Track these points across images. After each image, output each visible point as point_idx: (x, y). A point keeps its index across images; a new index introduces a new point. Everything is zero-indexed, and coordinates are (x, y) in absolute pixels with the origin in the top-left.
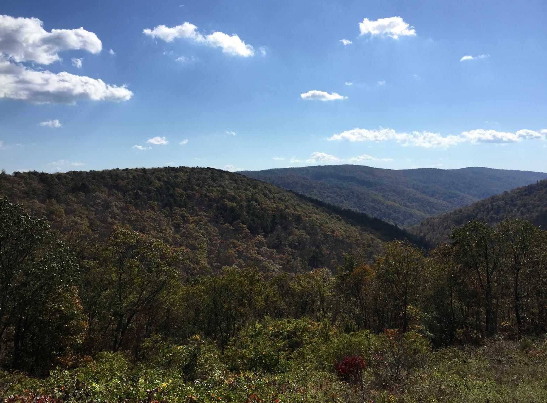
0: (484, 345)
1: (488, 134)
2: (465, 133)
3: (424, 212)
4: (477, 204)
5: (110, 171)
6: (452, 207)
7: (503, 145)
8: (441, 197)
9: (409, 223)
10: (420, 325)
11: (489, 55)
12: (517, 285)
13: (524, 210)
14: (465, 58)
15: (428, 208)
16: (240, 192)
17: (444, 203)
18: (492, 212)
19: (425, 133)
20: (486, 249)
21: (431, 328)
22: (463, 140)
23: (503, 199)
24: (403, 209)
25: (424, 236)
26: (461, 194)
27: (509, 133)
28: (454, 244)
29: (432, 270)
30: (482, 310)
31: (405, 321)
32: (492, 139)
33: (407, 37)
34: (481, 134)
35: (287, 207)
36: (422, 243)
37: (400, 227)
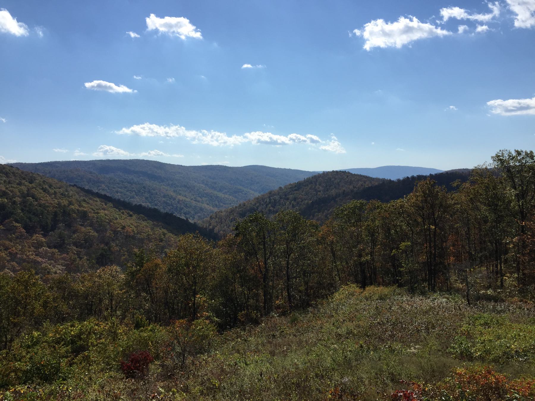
2: (247, 134)
3: (213, 206)
4: (258, 199)
7: (278, 146)
9: (199, 216)
12: (288, 268)
13: (295, 203)
14: (245, 66)
18: (270, 205)
19: (213, 133)
22: (246, 140)
24: (194, 203)
25: (213, 228)
27: (282, 136)
28: (237, 235)
29: (218, 257)
30: (261, 292)
31: (194, 310)
32: (269, 140)
33: (193, 38)
36: (210, 235)
37: (191, 221)
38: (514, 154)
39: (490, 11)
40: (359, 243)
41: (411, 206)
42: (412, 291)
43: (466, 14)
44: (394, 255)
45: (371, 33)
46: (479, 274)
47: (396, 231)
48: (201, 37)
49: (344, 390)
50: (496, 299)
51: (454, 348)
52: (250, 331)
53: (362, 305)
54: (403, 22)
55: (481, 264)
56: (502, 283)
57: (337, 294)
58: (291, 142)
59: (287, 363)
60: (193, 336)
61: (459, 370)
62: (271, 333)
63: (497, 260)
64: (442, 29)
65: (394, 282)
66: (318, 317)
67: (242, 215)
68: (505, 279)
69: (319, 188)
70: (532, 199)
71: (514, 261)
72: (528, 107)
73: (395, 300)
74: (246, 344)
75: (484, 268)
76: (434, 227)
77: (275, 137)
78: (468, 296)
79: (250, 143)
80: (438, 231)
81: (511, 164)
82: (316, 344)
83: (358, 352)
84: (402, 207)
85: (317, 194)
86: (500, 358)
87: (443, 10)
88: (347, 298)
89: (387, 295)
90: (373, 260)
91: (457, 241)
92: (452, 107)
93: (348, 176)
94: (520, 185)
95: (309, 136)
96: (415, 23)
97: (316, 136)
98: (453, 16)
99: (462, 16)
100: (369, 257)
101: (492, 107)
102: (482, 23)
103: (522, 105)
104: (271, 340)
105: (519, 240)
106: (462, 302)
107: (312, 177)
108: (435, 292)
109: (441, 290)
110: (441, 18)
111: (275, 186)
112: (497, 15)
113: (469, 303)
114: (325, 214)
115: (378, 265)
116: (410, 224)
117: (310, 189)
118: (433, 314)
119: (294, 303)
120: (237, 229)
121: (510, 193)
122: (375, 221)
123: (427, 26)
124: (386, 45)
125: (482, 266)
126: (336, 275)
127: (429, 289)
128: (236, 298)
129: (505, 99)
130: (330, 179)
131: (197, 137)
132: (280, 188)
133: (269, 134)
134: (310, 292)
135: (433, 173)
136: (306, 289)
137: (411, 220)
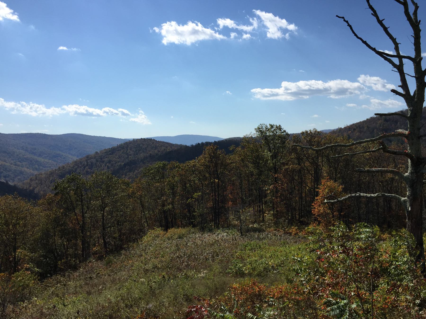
0: (80, 268)
1: (83, 109)
2: (65, 107)
3: (33, 170)
4: (76, 162)
6: (56, 165)
7: (93, 118)
8: (47, 157)
9: (19, 179)
10: (28, 264)
11: (80, 50)
12: (103, 219)
13: (110, 165)
14: (61, 48)
15: (37, 166)
17: (50, 161)
18: (87, 167)
19: (32, 105)
20: (82, 196)
21: (38, 264)
22: (64, 112)
23: (95, 157)
24: (13, 167)
25: (34, 189)
26: (64, 154)
27: (97, 110)
28: (56, 194)
29: (38, 215)
30: (79, 242)
31: (15, 264)
32: (85, 112)
33: (10, 21)
34: (77, 108)
36: (29, 195)
37: (11, 183)
38: (269, 127)
39: (251, 24)
40: (162, 195)
41: (201, 165)
42: (203, 230)
43: (235, 25)
44: (189, 203)
45: (168, 31)
46: (249, 213)
47: (190, 184)
48: (18, 20)
49: (149, 314)
50: (260, 230)
51: (231, 269)
52: (69, 276)
53: (165, 244)
54: (191, 26)
55: (250, 206)
56: (263, 219)
57: (146, 237)
58: (105, 115)
59: (101, 300)
60: (13, 286)
61: (236, 285)
62: (89, 276)
63: (260, 202)
64: (219, 34)
65: (190, 224)
66: (130, 258)
67: (62, 176)
68: (266, 216)
69: (130, 152)
70: (281, 158)
71: (271, 202)
72: (277, 95)
73: (190, 237)
74: (65, 288)
75: (251, 209)
76: (217, 181)
77: (91, 110)
78: (241, 230)
79: (67, 114)
80: (220, 183)
81: (267, 134)
82: (128, 280)
83: (161, 282)
84: (194, 166)
85: (128, 158)
86: (262, 272)
87: (219, 20)
88: (154, 239)
89: (184, 235)
90: (173, 208)
91: (233, 190)
92: (228, 92)
93: (153, 143)
94: (273, 149)
95: (120, 110)
96: (200, 27)
97: (126, 110)
98: (226, 25)
99: (232, 26)
100: (171, 206)
101: (254, 94)
102: (246, 33)
103: (273, 93)
104: (88, 282)
105: (273, 187)
106: (236, 234)
107: (124, 144)
108: (218, 228)
109: (223, 227)
110: (218, 26)
111: (91, 151)
112: (256, 28)
113: (242, 235)
114: (135, 173)
115: (178, 211)
116: (201, 179)
117: (123, 153)
118: (217, 245)
119: (109, 248)
120: (56, 188)
121: (267, 154)
122: (174, 177)
123: (209, 31)
124: (179, 42)
125: (250, 207)
126: (144, 222)
127: (215, 227)
128: (56, 249)
129: (263, 88)
130: (139, 145)
131: (16, 108)
132: (97, 153)
133: (86, 107)
134: (123, 237)
135: (217, 141)
136: (120, 236)
137: (202, 176)
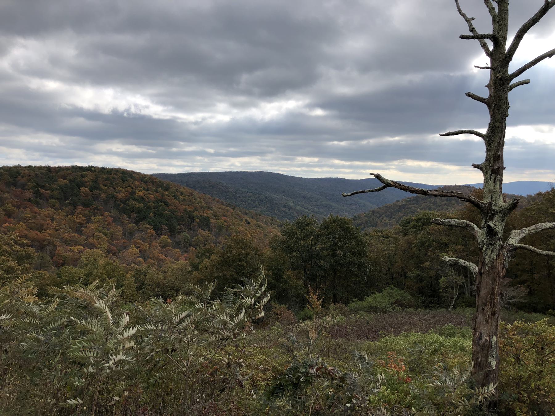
5: (10, 168)
16: (149, 194)
35: (196, 209)
